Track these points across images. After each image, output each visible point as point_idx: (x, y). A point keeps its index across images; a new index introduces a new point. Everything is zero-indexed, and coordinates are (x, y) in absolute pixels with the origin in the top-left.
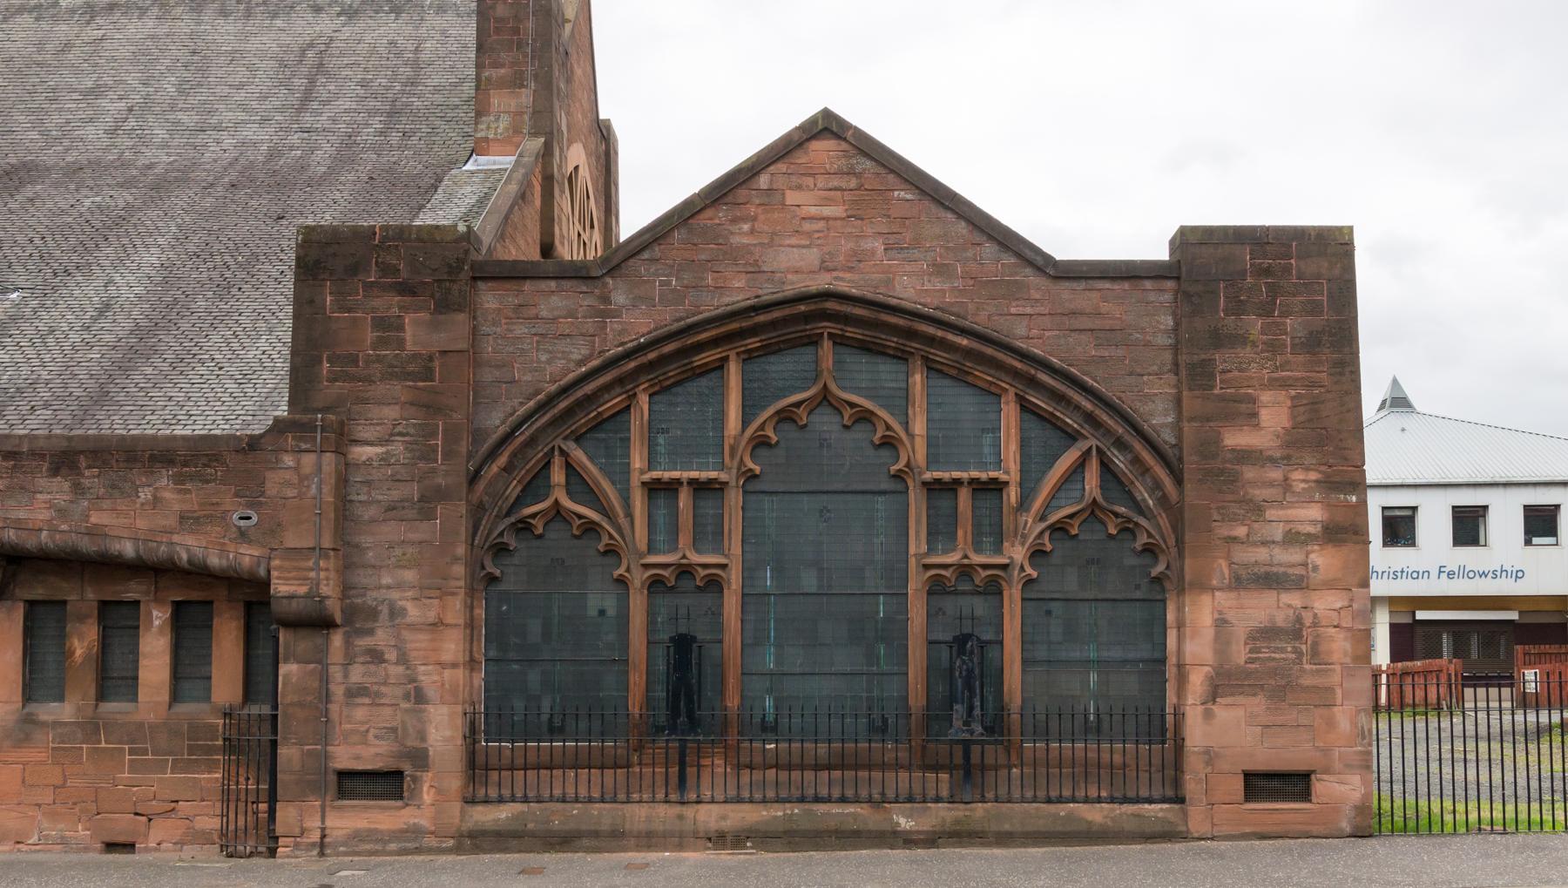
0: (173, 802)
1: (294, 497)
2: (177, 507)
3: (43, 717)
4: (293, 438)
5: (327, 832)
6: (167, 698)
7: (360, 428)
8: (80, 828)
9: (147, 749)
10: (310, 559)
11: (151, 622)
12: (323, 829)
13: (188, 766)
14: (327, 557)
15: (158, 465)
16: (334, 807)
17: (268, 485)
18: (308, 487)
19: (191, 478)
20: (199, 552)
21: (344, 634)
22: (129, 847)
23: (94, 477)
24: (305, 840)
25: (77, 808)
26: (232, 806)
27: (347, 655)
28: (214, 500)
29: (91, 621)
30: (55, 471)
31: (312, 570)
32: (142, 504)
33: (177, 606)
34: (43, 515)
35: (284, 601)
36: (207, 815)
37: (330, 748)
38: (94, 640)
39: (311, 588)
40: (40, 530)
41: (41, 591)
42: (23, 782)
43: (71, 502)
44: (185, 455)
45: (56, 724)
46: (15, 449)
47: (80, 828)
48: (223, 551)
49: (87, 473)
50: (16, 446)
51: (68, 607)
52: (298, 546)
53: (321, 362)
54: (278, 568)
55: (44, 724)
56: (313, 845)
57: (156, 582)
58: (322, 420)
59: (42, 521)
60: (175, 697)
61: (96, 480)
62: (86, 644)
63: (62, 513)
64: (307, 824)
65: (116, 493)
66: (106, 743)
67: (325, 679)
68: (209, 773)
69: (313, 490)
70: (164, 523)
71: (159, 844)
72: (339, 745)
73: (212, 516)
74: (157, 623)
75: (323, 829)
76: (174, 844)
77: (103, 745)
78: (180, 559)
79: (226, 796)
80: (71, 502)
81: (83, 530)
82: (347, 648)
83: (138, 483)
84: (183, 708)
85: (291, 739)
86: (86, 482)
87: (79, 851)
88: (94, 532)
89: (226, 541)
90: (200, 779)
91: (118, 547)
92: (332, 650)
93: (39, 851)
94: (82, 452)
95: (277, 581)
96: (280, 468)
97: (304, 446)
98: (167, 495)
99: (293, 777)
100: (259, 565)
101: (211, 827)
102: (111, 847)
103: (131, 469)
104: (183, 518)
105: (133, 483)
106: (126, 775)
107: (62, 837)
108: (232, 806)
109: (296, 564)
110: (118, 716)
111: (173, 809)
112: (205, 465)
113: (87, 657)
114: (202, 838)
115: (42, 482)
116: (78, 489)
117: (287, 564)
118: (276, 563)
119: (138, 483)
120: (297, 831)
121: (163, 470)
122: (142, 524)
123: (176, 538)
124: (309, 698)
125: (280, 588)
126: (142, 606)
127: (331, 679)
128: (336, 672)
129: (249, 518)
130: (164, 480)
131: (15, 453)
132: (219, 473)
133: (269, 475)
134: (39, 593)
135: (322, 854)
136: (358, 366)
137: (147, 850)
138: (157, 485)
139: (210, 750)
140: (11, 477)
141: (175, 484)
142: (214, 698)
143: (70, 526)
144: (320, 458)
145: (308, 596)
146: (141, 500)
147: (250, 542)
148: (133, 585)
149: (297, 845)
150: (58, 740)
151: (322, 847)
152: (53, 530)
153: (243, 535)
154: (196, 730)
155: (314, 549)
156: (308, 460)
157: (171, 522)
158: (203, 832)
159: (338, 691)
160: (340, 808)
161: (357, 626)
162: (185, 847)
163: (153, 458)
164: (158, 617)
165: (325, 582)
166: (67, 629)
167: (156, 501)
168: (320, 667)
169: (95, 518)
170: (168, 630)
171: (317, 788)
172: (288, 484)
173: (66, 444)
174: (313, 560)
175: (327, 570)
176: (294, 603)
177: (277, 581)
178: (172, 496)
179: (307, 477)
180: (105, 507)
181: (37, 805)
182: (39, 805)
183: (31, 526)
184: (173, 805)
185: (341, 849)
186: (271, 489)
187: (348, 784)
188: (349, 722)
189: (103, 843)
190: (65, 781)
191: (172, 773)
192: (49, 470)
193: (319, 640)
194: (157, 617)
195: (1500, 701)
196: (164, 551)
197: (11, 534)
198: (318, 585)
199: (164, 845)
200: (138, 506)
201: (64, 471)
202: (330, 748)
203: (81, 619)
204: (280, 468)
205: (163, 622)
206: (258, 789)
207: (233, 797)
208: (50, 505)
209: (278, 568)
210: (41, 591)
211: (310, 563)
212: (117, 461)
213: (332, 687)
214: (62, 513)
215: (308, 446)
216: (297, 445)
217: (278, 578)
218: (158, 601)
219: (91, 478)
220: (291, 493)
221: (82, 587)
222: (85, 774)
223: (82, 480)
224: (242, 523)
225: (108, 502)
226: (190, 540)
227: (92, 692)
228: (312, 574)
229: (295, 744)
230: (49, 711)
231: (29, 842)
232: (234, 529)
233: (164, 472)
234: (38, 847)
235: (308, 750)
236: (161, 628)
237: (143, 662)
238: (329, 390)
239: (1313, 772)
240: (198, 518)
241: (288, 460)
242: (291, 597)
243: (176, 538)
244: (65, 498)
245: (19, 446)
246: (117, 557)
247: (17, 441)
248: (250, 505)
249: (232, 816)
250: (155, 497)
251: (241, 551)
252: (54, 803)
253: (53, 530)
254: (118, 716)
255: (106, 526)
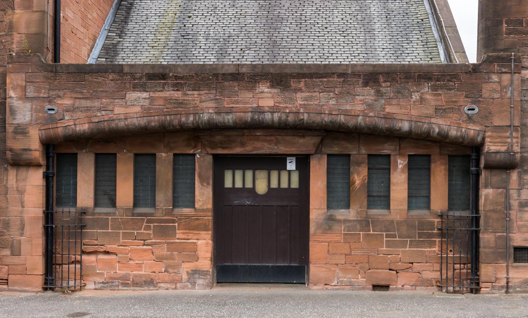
0: (410, 263)
1: (498, 98)
2: (433, 103)
3: (339, 217)
4: (498, 66)
5: (510, 280)
6: (406, 207)
7: (525, 60)
8: (360, 277)
9: (396, 235)
10: (508, 132)
11: (397, 166)
12: (508, 279)
13: (418, 244)
14: (517, 131)
15: (423, 80)
16: (513, 267)
17: (484, 91)
18: (506, 92)
19: (441, 87)
20: (445, 128)
21: (518, 172)
22: (386, 287)
23: (388, 87)
24: (497, 284)
25: (358, 267)
26: (444, 266)
27: (520, 184)
28: (454, 100)
29: (363, 165)
30: (366, 84)
31: (509, 138)
32: (414, 102)
33: (411, 157)
34: (360, 108)
35: (493, 154)
36: (429, 270)
37: (511, 235)
38: (366, 176)
39: (508, 148)
40: (358, 116)
41: (336, 149)
42: (328, 251)
43: (375, 100)
44: (437, 75)
45: (345, 221)
46: (344, 72)
47: (360, 277)
48: (459, 127)
49: (384, 85)
50: (344, 70)
51: (351, 158)
52: (501, 125)
53: (502, 24)
54: (490, 137)
55: (339, 221)
56: (502, 287)
57: (400, 145)
58: (514, 56)
59: (359, 111)
60: (410, 207)
61: (389, 89)
62: (361, 178)
63: (370, 106)
64: (499, 276)
65: (400, 96)
66: (373, 231)
67: (507, 197)
68: (430, 248)
69: (509, 94)
70: (427, 112)
71: (403, 286)
72: (516, 233)
73: (453, 108)
74: (400, 166)
75: (508, 279)
76: (412, 286)
77: (371, 232)
78: (433, 132)
79: (442, 261)
80: (375, 100)
81: (382, 116)
82: (520, 180)
83: (412, 90)
84: (416, 213)
85: (489, 229)
86: (383, 90)
87: (359, 289)
88: (387, 117)
89: (461, 122)
90: (425, 251)
91: (400, 125)
92: (511, 181)
93: (338, 289)
94: (380, 73)
95: (489, 144)
96: (490, 82)
97: (504, 70)
98: (428, 97)
99: (491, 250)
100: (478, 135)
101: (431, 277)
102: (376, 287)
103: (408, 83)
104: (436, 110)
105: (409, 90)
106: (384, 249)
107: (350, 282)
108: (444, 266)
109: (498, 134)
110: (380, 217)
111: (411, 267)
112: (448, 81)
113: (362, 185)
114: (427, 283)
115: (359, 90)
116: (379, 94)
117: (495, 134)
118: (488, 134)
119: (412, 90)
120: (493, 279)
121: (426, 83)
122: (414, 112)
123: (433, 120)
124: (499, 208)
125: (490, 147)
126: (392, 158)
127: (511, 197)
128: (514, 193)
129: (473, 109)
130: (426, 88)
131: (344, 74)
132: (456, 85)
133: (484, 86)
134: (336, 150)
135: (507, 292)
136: (522, 26)
137: (397, 289)
138: (422, 91)
139: (431, 235)
140: (342, 87)
141: (432, 91)
142: (433, 207)
143: (374, 113)
144: (512, 77)
145: (507, 152)
146: (413, 100)
147: (474, 122)
148: (386, 146)
149: (493, 287)
150: (347, 229)
151: (507, 288)
152: (365, 116)
153: (470, 118)
154: (423, 225)
155: (510, 126)
156: (506, 78)
157: (431, 111)
158: (427, 280)
159: (515, 204)
160: (517, 267)
161: (525, 168)
162: (417, 288)
163: (420, 77)
164: (401, 163)
165: (516, 144)
166: (351, 169)
167: (422, 100)
168: (505, 190)
169: (388, 109)
170: (406, 170)
171: (504, 257)
172: (495, 91)
173: (371, 69)
174: (510, 132)
175: (517, 138)
176: (498, 156)
177: (489, 144)
178: (431, 97)
179: (505, 87)
180: (394, 103)
181: (336, 264)
182: (337, 265)
183: (353, 114)
184: (411, 265)
185: (518, 289)
186: (485, 93)
187: (519, 254)
188: (521, 221)
189: (372, 285)
190: (351, 252)
191: (409, 248)
192: (363, 83)
193: (504, 176)
194: (400, 164)
195: (75, 267)
196: (426, 128)
197: (342, 118)
198: (512, 146)
199: (406, 287)
200: (412, 103)
201: (371, 83)
202: (511, 235)
203: (359, 164)
204: (490, 82)
205: (404, 166)
206: (442, 256)
207: (444, 261)
208: (364, 102)
209: (490, 137)
210: (336, 149)
211: (508, 134)
212: (400, 78)
213: (512, 201)
214: (370, 106)
215: (506, 70)
216: (500, 69)
217: (490, 142)
218: (401, 155)
219: (386, 87)
220: (496, 96)
221: (359, 147)
222: (362, 248)
223: (381, 89)
224: (470, 112)
225: (395, 100)
226: (441, 122)
227: (365, 203)
228: (509, 140)
229: (492, 232)
230: (341, 214)
231: (333, 284)
232: (465, 116)
233: (426, 84)
234: (337, 287)
235: (499, 236)
236: (402, 169)
237: (392, 188)
238: (506, 40)
239: (390, 285)
240: (445, 110)
241: (495, 78)
242: (497, 153)
243: (433, 120)
244: (371, 98)
245: (346, 70)
246: (398, 130)
247: (345, 68)
248: (474, 103)
249: (444, 271)
250: (421, 98)
251: (469, 127)
252: (345, 264)
253: (365, 116)
254: (380, 217)
255: (394, 114)
